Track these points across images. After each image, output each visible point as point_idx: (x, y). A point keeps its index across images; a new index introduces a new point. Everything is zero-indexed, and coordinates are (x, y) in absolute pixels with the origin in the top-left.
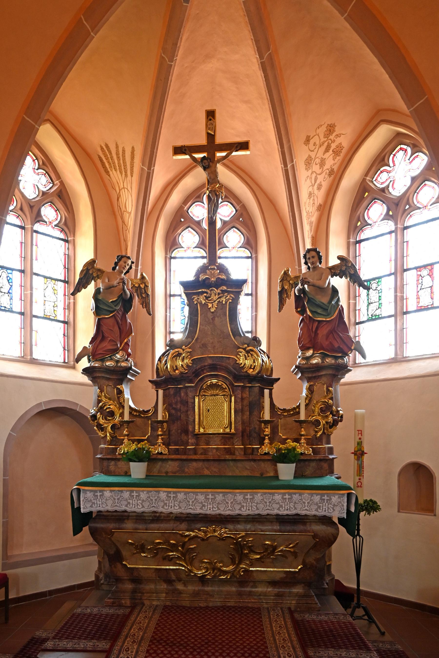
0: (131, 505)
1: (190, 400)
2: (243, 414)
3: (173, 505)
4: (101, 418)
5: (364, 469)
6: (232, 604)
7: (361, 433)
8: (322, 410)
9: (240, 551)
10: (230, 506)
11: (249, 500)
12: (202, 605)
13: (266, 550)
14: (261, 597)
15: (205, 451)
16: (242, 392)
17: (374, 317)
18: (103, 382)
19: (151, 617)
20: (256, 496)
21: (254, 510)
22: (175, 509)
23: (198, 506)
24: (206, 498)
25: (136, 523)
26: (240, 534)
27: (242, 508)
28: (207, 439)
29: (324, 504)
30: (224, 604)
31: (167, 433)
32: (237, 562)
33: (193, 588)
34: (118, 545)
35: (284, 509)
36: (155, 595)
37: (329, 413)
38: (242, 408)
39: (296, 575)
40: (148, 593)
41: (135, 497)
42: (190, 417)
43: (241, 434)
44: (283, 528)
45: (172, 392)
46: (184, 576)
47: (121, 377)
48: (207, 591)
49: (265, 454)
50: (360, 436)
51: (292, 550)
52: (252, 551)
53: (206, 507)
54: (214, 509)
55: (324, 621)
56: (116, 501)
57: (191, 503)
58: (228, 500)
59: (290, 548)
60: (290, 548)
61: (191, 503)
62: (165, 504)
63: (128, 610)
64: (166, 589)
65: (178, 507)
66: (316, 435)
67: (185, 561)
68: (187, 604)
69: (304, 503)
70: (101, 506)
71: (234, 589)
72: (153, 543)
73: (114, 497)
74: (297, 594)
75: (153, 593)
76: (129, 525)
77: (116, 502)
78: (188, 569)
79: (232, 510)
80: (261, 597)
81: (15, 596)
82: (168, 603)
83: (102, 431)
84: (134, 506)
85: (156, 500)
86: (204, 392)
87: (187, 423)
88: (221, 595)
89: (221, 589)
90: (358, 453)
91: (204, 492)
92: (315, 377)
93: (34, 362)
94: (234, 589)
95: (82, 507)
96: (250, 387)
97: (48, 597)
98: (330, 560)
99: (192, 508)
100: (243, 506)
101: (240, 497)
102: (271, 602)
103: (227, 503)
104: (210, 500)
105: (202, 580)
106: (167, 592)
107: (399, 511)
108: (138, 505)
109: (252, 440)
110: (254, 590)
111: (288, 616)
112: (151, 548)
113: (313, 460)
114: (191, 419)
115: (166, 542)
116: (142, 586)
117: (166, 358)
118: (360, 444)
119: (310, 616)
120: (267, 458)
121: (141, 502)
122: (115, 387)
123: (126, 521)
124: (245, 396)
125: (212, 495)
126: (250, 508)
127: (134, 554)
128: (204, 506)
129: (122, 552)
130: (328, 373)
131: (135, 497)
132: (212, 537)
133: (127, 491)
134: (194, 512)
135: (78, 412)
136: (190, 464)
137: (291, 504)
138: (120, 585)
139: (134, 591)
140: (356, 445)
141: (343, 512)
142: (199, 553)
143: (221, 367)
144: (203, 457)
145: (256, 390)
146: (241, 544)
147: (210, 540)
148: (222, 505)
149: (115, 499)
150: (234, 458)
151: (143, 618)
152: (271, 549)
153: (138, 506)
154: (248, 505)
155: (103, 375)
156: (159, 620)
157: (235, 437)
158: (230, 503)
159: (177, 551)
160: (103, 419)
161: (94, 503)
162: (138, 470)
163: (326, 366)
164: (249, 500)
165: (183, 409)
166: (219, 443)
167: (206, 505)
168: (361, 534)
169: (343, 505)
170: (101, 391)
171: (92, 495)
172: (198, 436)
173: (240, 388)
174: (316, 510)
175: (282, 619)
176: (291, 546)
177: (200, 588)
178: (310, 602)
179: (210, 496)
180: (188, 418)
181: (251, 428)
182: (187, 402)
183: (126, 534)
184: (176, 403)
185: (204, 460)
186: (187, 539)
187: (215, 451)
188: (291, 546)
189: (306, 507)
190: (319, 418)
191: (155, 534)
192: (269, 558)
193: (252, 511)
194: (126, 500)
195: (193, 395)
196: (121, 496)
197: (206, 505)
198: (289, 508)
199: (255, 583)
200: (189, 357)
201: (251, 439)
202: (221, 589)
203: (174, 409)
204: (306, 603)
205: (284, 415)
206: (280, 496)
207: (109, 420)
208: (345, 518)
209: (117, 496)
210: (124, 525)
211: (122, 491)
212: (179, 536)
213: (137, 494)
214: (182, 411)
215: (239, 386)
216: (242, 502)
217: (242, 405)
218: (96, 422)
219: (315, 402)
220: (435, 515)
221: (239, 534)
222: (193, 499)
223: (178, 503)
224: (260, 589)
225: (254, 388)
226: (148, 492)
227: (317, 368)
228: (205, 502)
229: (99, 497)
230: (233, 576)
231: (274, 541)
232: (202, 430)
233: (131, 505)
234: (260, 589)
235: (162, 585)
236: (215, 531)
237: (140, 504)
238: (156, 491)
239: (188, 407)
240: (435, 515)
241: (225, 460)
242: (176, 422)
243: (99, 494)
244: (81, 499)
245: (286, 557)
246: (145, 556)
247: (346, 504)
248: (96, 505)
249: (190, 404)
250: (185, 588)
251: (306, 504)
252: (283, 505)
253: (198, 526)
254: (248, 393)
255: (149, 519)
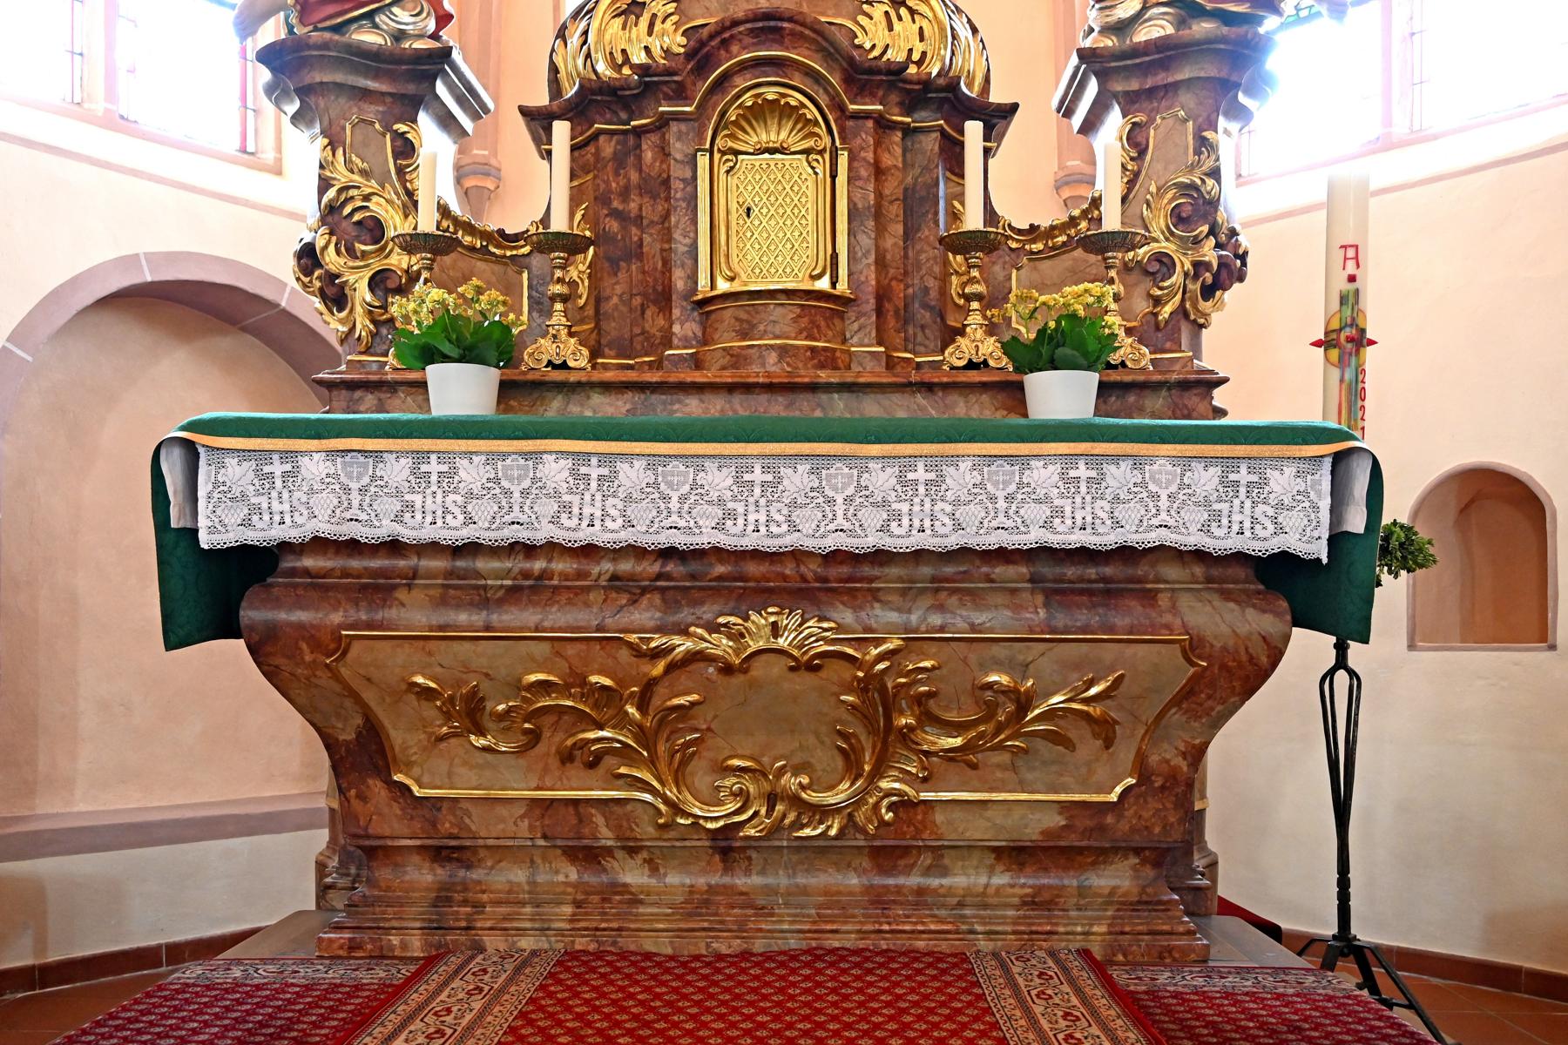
0: (419, 516)
1: (678, 172)
2: (880, 230)
3: (598, 513)
4: (332, 248)
5: (1366, 403)
6: (850, 942)
7: (1357, 258)
8: (1179, 218)
9: (881, 716)
10: (840, 513)
11: (922, 489)
12: (724, 950)
13: (990, 710)
14: (967, 912)
15: (737, 359)
16: (878, 144)
17: (1303, 14)
18: (337, 106)
19: (502, 990)
20: (952, 470)
21: (942, 530)
22: (605, 529)
23: (703, 515)
24: (738, 480)
25: (443, 602)
26: (884, 640)
27: (894, 524)
28: (743, 316)
29: (1237, 502)
30: (814, 944)
31: (590, 311)
32: (867, 768)
33: (688, 881)
34: (369, 696)
35: (1069, 522)
36: (528, 909)
37: (1205, 228)
38: (878, 206)
39: (1109, 819)
40: (498, 903)
41: (434, 478)
42: (677, 235)
43: (873, 301)
44: (1061, 619)
45: (608, 147)
46: (651, 830)
47: (411, 88)
48: (742, 894)
49: (971, 365)
50: (1351, 268)
51: (1095, 710)
52: (929, 718)
53: (740, 521)
54: (774, 529)
55: (1247, 994)
56: (356, 498)
57: (674, 504)
58: (836, 490)
59: (1087, 701)
60: (1087, 701)
61: (674, 504)
62: (566, 507)
63: (406, 970)
64: (575, 886)
65: (620, 521)
66: (1156, 315)
67: (652, 763)
68: (662, 945)
69: (1155, 497)
70: (288, 519)
71: (854, 881)
72: (517, 687)
73: (343, 479)
74: (1111, 897)
75: (523, 904)
76: (413, 613)
77: (355, 503)
78: (666, 801)
79: (851, 533)
80: (967, 912)
81: (29, 962)
82: (581, 943)
83: (340, 310)
84: (429, 519)
85: (525, 493)
86: (732, 136)
87: (666, 263)
88: (800, 904)
89: (801, 880)
90: (1343, 336)
91: (730, 457)
92: (1151, 93)
93: (120, 124)
94: (855, 881)
95: (203, 523)
96: (908, 131)
97: (163, 969)
98: (1203, 797)
99: (682, 523)
100: (898, 517)
101: (883, 476)
102: (1009, 928)
103: (831, 501)
104: (757, 491)
105: (726, 846)
106: (580, 897)
107: (1412, 646)
108: (446, 511)
109: (915, 335)
110: (935, 882)
111: (1087, 979)
112: (509, 710)
113: (1158, 386)
114: (680, 245)
115: (576, 681)
116: (475, 875)
117: (583, 24)
118: (1350, 299)
119: (1178, 978)
120: (977, 379)
121: (459, 499)
122: (388, 128)
123: (401, 594)
124: (887, 160)
125: (765, 469)
126: (927, 523)
127: (441, 739)
128: (731, 515)
129: (393, 733)
130: (1202, 74)
131: (434, 478)
132: (764, 657)
133: (400, 454)
134: (689, 540)
135: (284, 311)
136: (676, 406)
137: (1099, 503)
138: (384, 874)
139: (443, 897)
140: (1335, 305)
141: (1316, 534)
142: (709, 729)
143: (799, 28)
144: (728, 377)
145: (931, 143)
146: (884, 687)
147: (758, 669)
148: (807, 512)
149: (347, 490)
150: (849, 380)
151: (461, 996)
152: (1011, 708)
153: (449, 517)
154: (916, 508)
155: (339, 77)
156: (532, 1000)
157: (851, 315)
158: (840, 501)
159: (622, 721)
160: (338, 253)
161: (258, 509)
162: (459, 389)
163: (1198, 43)
164: (922, 489)
165: (652, 211)
166: (791, 330)
167: (741, 510)
168: (1351, 663)
169: (1316, 508)
170: (333, 145)
171: (251, 475)
172: (705, 306)
173: (870, 124)
174: (1205, 529)
175: (1066, 988)
176: (1093, 691)
177: (715, 879)
178: (1166, 928)
179: (758, 475)
180: (670, 240)
181: (910, 291)
182: (666, 183)
183: (405, 649)
184: (625, 194)
185: (731, 388)
186: (659, 668)
187: (772, 357)
188: (1093, 691)
189: (1163, 515)
190: (1169, 247)
191: (520, 650)
192: (1000, 747)
193: (935, 534)
194: (399, 493)
195: (691, 151)
196: (373, 478)
197: (741, 510)
198: (1089, 519)
199: (940, 855)
200: (675, 18)
201: (911, 331)
202: (801, 880)
203: (615, 214)
204: (1150, 933)
205: (1032, 253)
206: (1054, 469)
207: (364, 255)
208: (1325, 561)
209: (359, 478)
210: (392, 613)
211: (377, 455)
212: (624, 655)
213: (444, 468)
214: (645, 222)
215: (866, 115)
216: (892, 497)
217: (879, 195)
218: (316, 274)
219: (1153, 189)
220: (1553, 647)
221: (878, 642)
222: (686, 488)
223: (620, 505)
224: (963, 879)
225: (922, 137)
226: (492, 457)
227: (1165, 53)
228: (734, 499)
229: (279, 483)
230: (850, 824)
231: (1024, 669)
232: (723, 286)
233: (419, 516)
234: (963, 879)
235: (557, 872)
236: (776, 630)
237: (457, 511)
238: (526, 455)
239: (668, 199)
240: (1553, 647)
241: (813, 388)
242: (623, 264)
243: (277, 468)
244: (201, 493)
245: (1068, 744)
246: (485, 749)
247: (1329, 500)
248: (266, 517)
249: (677, 185)
250: (653, 881)
251: (1164, 503)
252: (1068, 509)
253: (707, 612)
254: (898, 151)
255: (502, 586)
